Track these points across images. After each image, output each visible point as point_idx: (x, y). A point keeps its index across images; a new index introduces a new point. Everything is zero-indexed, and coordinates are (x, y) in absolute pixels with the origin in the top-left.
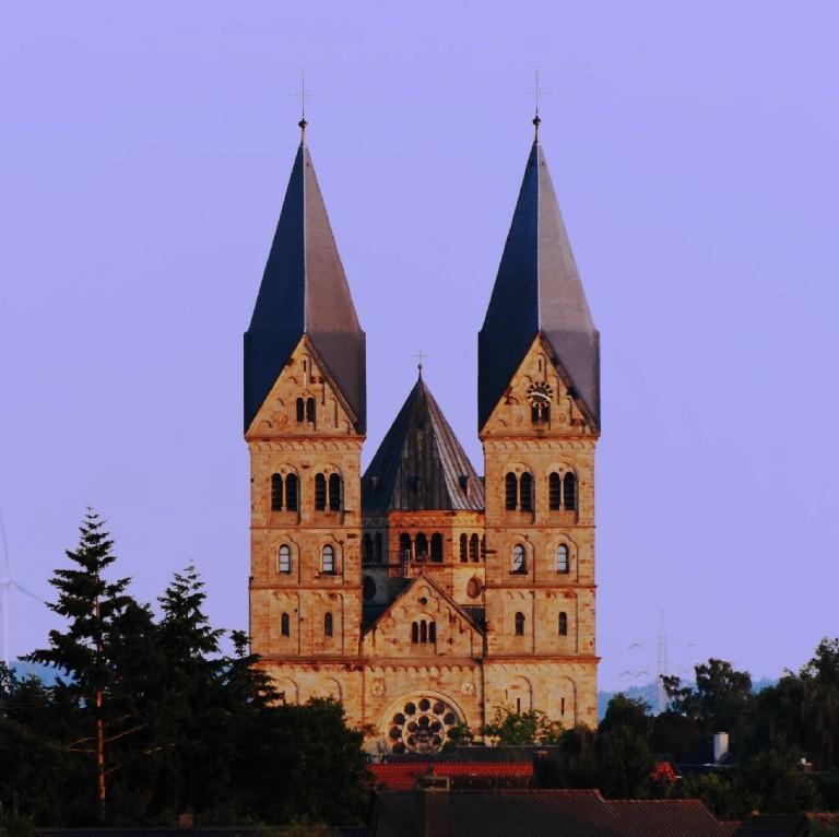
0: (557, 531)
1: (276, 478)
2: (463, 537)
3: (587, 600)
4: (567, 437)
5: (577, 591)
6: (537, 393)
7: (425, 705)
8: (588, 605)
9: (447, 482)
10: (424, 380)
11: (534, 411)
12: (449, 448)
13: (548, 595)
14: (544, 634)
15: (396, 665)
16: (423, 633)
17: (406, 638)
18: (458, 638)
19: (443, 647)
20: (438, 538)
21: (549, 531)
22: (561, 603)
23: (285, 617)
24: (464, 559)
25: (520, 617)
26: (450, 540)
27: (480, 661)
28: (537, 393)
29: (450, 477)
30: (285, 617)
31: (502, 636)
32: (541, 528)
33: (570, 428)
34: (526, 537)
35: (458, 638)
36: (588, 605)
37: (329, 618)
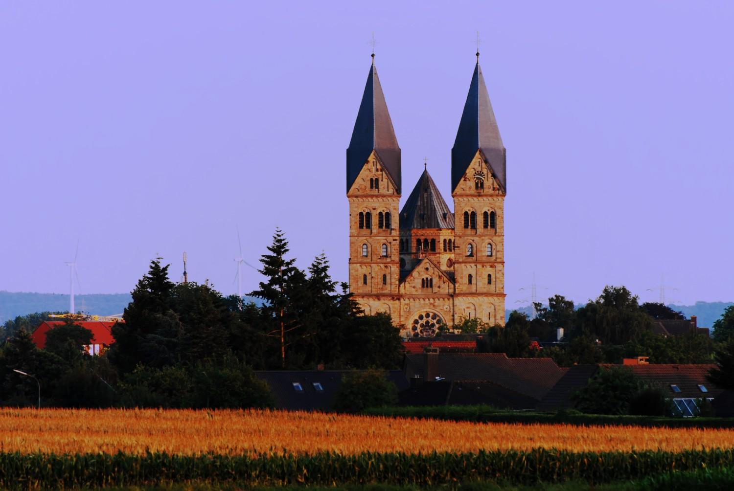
0: (487, 237)
1: (361, 214)
2: (445, 240)
3: (500, 269)
4: (491, 196)
5: (496, 264)
6: (478, 176)
7: (428, 315)
8: (501, 271)
9: (438, 216)
10: (427, 169)
11: (477, 184)
12: (438, 200)
13: (483, 266)
14: (481, 284)
15: (414, 298)
16: (427, 283)
17: (419, 285)
18: (442, 285)
19: (436, 289)
20: (433, 241)
21: (483, 237)
22: (488, 270)
23: (365, 276)
24: (445, 250)
25: (470, 276)
26: (439, 242)
27: (452, 296)
28: (478, 176)
29: (439, 214)
30: (365, 276)
31: (462, 285)
32: (480, 236)
33: (493, 192)
34: (473, 240)
35: (442, 285)
36: (501, 271)
37: (385, 276)
